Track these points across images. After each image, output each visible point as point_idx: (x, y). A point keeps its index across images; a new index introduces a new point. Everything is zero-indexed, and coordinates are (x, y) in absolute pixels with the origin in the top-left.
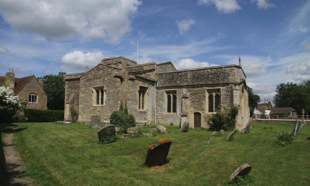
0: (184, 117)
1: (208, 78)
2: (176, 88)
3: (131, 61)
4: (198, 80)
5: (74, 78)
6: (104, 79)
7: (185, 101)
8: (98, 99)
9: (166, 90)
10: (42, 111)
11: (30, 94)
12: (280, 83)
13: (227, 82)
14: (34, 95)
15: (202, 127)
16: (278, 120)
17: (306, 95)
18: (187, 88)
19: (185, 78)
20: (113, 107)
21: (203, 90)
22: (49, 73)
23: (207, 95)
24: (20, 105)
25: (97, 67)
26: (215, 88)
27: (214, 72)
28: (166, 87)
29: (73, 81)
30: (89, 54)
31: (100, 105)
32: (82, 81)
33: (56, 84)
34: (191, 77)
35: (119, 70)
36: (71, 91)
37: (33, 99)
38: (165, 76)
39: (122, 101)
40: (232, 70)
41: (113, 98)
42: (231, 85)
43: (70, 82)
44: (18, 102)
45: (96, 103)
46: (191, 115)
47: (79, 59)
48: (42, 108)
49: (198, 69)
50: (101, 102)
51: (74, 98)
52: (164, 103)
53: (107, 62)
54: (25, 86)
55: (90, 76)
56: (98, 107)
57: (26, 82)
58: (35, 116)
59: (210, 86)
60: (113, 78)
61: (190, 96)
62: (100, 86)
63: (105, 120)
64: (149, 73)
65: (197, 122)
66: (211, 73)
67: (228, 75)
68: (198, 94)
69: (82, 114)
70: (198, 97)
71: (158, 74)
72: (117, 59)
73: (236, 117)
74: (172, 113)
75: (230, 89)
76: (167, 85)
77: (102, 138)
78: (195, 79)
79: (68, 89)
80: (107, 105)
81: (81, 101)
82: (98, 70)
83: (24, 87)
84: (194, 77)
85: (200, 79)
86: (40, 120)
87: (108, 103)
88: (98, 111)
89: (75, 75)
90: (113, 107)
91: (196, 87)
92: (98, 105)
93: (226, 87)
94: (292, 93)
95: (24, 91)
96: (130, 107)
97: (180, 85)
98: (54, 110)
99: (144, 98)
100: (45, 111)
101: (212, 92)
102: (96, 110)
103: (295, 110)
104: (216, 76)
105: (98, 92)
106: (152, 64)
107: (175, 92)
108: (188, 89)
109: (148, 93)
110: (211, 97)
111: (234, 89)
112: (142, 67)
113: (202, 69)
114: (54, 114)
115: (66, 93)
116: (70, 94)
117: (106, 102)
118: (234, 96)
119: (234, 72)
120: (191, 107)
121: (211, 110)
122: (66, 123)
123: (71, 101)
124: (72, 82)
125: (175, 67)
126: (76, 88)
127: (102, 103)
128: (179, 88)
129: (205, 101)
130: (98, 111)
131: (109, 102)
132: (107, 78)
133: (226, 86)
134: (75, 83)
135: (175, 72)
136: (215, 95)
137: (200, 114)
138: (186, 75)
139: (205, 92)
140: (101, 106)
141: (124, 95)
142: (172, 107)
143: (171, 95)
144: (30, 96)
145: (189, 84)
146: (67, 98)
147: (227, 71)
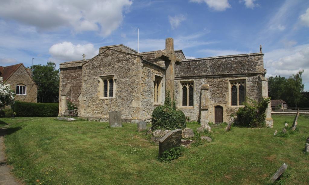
0: (204, 111)
2: (193, 79)
3: (132, 50)
5: (70, 67)
7: (205, 93)
8: (106, 90)
9: (182, 81)
10: (32, 104)
11: (18, 85)
13: (253, 72)
14: (23, 86)
16: (284, 112)
17: (295, 88)
18: (206, 78)
19: (204, 68)
20: (126, 100)
21: (225, 81)
22: (36, 63)
23: (230, 86)
24: (12, 97)
25: (105, 52)
26: (239, 79)
27: (238, 60)
28: (181, 77)
29: (68, 70)
30: (79, 46)
31: (108, 97)
32: (85, 69)
33: (44, 75)
34: (210, 66)
35: (134, 56)
36: (67, 81)
37: (20, 90)
39: (169, 92)
40: (259, 59)
41: (126, 89)
42: (258, 75)
43: (65, 72)
44: (10, 93)
45: (103, 95)
46: (211, 109)
47: (65, 51)
48: (32, 101)
49: (219, 57)
50: (110, 94)
52: (180, 96)
54: (11, 75)
55: (95, 63)
56: (106, 100)
57: (14, 70)
58: (25, 110)
59: (233, 77)
60: (125, 66)
61: (210, 87)
62: (109, 75)
64: (161, 62)
65: (219, 116)
68: (220, 86)
73: (266, 110)
74: (188, 107)
75: (258, 80)
77: (165, 150)
78: (216, 69)
79: (63, 79)
80: (118, 97)
81: (83, 93)
82: (105, 56)
83: (10, 76)
85: (221, 68)
86: (30, 115)
87: (119, 95)
88: (106, 105)
89: (72, 63)
90: (126, 100)
92: (106, 98)
93: (252, 77)
94: (282, 85)
95: (11, 81)
96: (146, 100)
98: (43, 103)
99: (158, 89)
100: (35, 104)
101: (186, 84)
102: (103, 103)
103: (285, 103)
104: (241, 66)
105: (105, 82)
107: (192, 83)
108: (208, 79)
109: (162, 84)
110: (234, 89)
111: (262, 80)
112: (152, 55)
113: (224, 57)
114: (46, 108)
115: (61, 84)
116: (65, 84)
117: (116, 94)
118: (263, 88)
119: (261, 61)
120: (211, 100)
121: (234, 103)
122: (70, 120)
123: (68, 93)
124: (68, 71)
125: (185, 56)
126: (73, 78)
127: (111, 95)
128: (197, 78)
129: (228, 93)
130: (106, 105)
131: (121, 94)
132: (118, 65)
133: (252, 76)
134: (72, 73)
135: (192, 61)
136: (240, 86)
137: (222, 108)
138: (205, 64)
139: (227, 83)
140: (110, 99)
141: (171, 83)
143: (188, 87)
144: (18, 87)
146: (61, 90)
147: (253, 60)
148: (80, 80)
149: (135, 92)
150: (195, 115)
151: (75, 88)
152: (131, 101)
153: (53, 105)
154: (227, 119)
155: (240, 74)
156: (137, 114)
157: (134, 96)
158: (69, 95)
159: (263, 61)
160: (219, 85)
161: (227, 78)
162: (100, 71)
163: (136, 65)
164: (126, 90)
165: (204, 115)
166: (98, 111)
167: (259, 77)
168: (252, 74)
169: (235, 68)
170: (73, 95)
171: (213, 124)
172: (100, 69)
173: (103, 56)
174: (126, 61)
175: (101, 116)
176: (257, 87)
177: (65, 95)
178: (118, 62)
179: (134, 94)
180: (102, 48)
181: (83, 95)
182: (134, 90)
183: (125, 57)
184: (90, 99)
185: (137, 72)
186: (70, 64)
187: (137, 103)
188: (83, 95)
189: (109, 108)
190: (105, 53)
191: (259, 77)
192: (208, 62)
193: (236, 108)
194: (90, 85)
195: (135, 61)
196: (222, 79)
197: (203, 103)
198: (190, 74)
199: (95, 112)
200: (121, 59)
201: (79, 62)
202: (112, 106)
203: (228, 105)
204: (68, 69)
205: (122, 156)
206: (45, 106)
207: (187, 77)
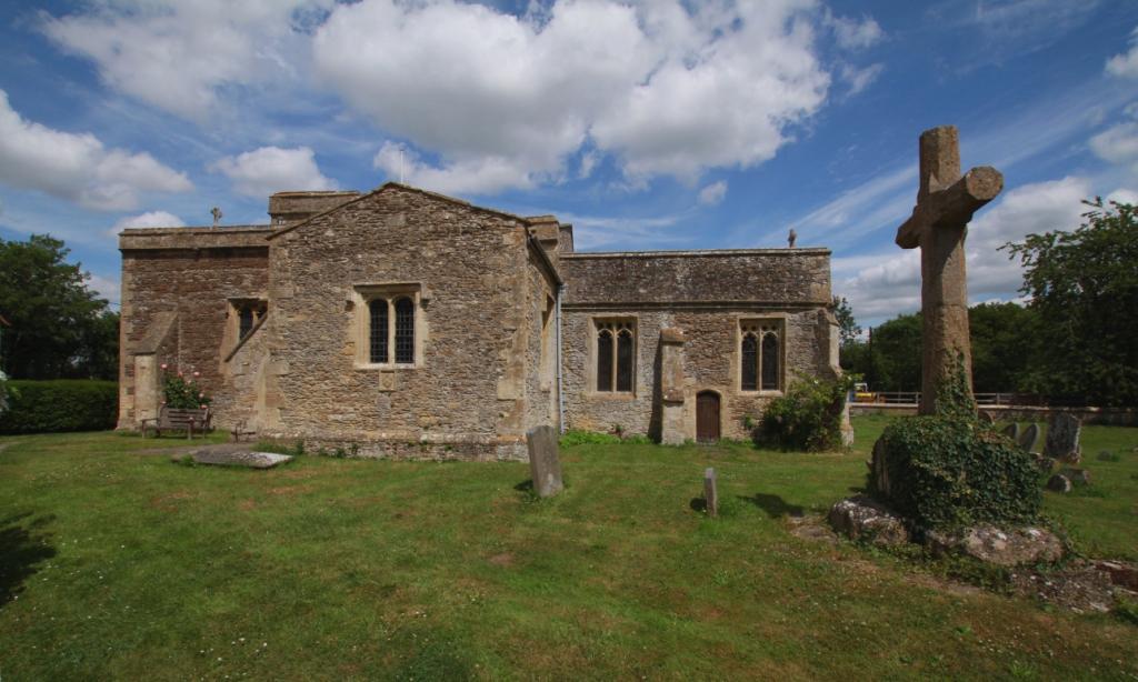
0: (670, 406)
1: (745, 284)
2: (635, 310)
4: (712, 290)
9: (599, 315)
12: (900, 316)
19: (667, 280)
21: (728, 320)
23: (595, 334)
26: (768, 317)
29: (164, 257)
31: (392, 364)
32: (281, 256)
34: (686, 278)
36: (157, 301)
38: (594, 266)
40: (819, 265)
42: (819, 308)
43: (146, 264)
51: (176, 330)
52: (590, 359)
53: (295, 206)
55: (330, 233)
56: (381, 374)
59: (750, 310)
62: (395, 282)
63: (426, 428)
68: (713, 334)
71: (566, 259)
74: (616, 394)
76: (602, 297)
79: (139, 289)
80: (434, 364)
82: (377, 212)
84: (700, 276)
87: (438, 355)
88: (382, 392)
89: (180, 234)
92: (380, 366)
93: (802, 314)
97: (650, 300)
101: (610, 327)
102: (371, 386)
105: (377, 308)
106: (546, 220)
107: (630, 323)
114: (51, 398)
116: (148, 312)
117: (429, 353)
119: (824, 272)
121: (749, 382)
122: (266, 463)
123: (163, 344)
124: (161, 263)
126: (183, 288)
127: (406, 353)
128: (646, 310)
129: (736, 355)
131: (449, 354)
132: (435, 249)
133: (801, 310)
134: (180, 270)
135: (630, 258)
136: (619, 334)
137: (716, 397)
138: (669, 269)
139: (734, 328)
142: (616, 370)
143: (615, 334)
145: (681, 300)
146: (130, 331)
148: (216, 298)
149: (509, 347)
150: (637, 418)
151: (195, 325)
152: (492, 378)
153: (81, 387)
154: (730, 428)
156: (515, 426)
157: (502, 363)
158: (171, 352)
161: (733, 314)
163: (512, 255)
164: (468, 341)
165: (673, 418)
166: (348, 416)
167: (821, 315)
168: (800, 304)
169: (757, 285)
170: (186, 352)
171: (693, 445)
172: (353, 260)
174: (468, 235)
175: (362, 432)
178: (433, 236)
179: (504, 354)
180: (282, 198)
181: (273, 354)
182: (502, 340)
183: (464, 222)
184: (310, 368)
185: (515, 276)
187: (516, 385)
188: (273, 354)
190: (377, 202)
191: (819, 315)
193: (757, 398)
194: (309, 315)
195: (508, 239)
196: (719, 315)
197: (667, 383)
198: (623, 296)
199: (332, 417)
200: (448, 229)
201: (213, 233)
202: (409, 395)
203: (733, 393)
205: (564, 628)
206: (43, 392)
207: (616, 305)
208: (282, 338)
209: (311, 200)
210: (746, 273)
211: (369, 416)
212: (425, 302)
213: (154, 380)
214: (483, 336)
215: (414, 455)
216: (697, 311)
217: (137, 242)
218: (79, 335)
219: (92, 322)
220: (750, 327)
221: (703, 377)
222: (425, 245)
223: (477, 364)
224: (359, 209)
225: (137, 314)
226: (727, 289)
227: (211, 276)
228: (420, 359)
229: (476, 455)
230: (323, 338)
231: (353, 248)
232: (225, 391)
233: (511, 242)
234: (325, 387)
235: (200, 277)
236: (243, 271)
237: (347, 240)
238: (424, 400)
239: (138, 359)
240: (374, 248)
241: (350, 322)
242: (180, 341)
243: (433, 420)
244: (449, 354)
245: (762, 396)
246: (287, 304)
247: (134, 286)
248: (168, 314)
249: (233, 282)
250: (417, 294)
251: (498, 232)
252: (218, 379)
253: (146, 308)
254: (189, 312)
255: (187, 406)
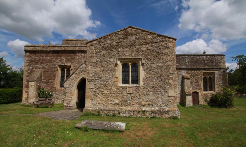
0: (188, 96)
4: (196, 64)
6: (139, 48)
7: (187, 81)
15: (200, 104)
18: (186, 70)
19: (184, 62)
21: (200, 73)
26: (210, 72)
36: (35, 66)
40: (222, 59)
42: (223, 70)
43: (32, 55)
51: (41, 74)
53: (69, 43)
55: (109, 42)
56: (127, 88)
59: (206, 70)
62: (132, 57)
63: (144, 106)
66: (206, 59)
67: (220, 62)
68: (196, 76)
69: (93, 97)
70: (196, 78)
72: (82, 41)
75: (223, 73)
79: (30, 62)
80: (146, 84)
82: (125, 35)
88: (128, 94)
89: (43, 46)
91: (195, 70)
93: (219, 71)
102: (124, 92)
105: (125, 66)
116: (32, 69)
117: (144, 81)
119: (224, 60)
124: (37, 55)
127: (135, 80)
128: (179, 70)
130: (128, 94)
131: (152, 81)
133: (219, 70)
134: (43, 57)
146: (27, 74)
148: (54, 65)
149: (172, 79)
151: (47, 73)
152: (166, 89)
153: (8, 91)
154: (202, 102)
155: (211, 68)
159: (225, 60)
160: (195, 76)
161: (202, 71)
162: (117, 52)
163: (172, 50)
164: (158, 77)
165: (189, 99)
169: (207, 64)
172: (117, 50)
173: (122, 34)
174: (157, 43)
176: (222, 78)
177: (35, 81)
180: (66, 40)
184: (102, 86)
185: (173, 56)
186: (39, 47)
187: (175, 91)
189: (133, 98)
190: (126, 32)
192: (186, 58)
197: (186, 89)
199: (110, 102)
200: (150, 41)
201: (53, 46)
202: (137, 95)
203: (202, 93)
204: (37, 52)
208: (92, 76)
209: (74, 41)
210: (204, 60)
211: (123, 102)
212: (143, 64)
213: (35, 89)
214: (163, 76)
215: (140, 115)
216: (192, 70)
217: (30, 49)
218: (3, 77)
219: (7, 73)
220: (210, 74)
221: (194, 88)
222: (142, 46)
223: (161, 85)
224: (119, 34)
225: (29, 70)
226: (200, 64)
227: (53, 59)
228: (141, 83)
229: (162, 115)
230: (107, 76)
231: (117, 47)
232: (56, 92)
233: (172, 46)
234: (107, 92)
235: (49, 59)
236: (62, 57)
237: (115, 44)
238: (143, 97)
239: (30, 83)
240: (125, 47)
241: (116, 70)
242: (42, 77)
243: (146, 103)
244: (152, 81)
245: (209, 93)
246: (94, 65)
247: (28, 61)
248: (39, 70)
249: (59, 61)
250: (140, 62)
251: (167, 43)
252: (54, 89)
253: (32, 68)
254: (45, 69)
255: (44, 96)
